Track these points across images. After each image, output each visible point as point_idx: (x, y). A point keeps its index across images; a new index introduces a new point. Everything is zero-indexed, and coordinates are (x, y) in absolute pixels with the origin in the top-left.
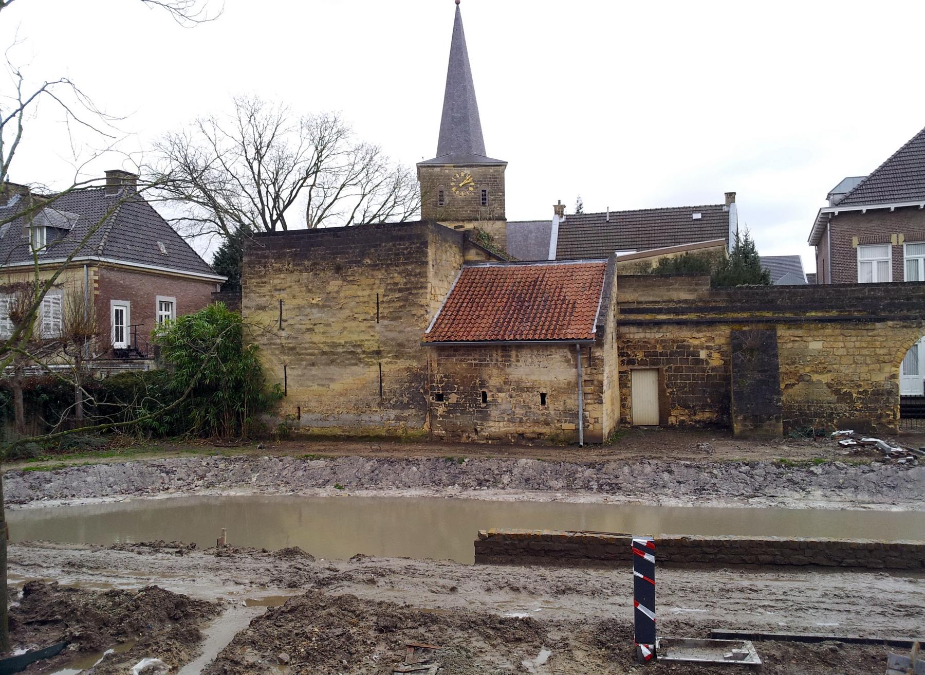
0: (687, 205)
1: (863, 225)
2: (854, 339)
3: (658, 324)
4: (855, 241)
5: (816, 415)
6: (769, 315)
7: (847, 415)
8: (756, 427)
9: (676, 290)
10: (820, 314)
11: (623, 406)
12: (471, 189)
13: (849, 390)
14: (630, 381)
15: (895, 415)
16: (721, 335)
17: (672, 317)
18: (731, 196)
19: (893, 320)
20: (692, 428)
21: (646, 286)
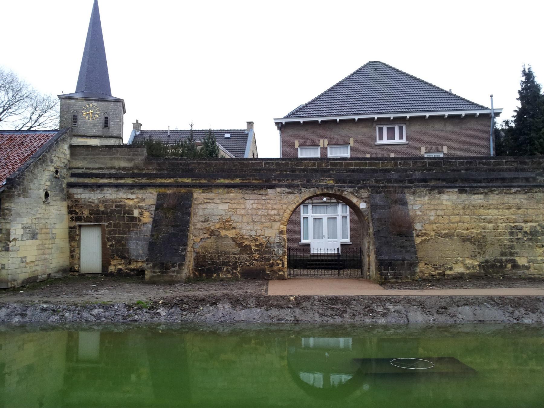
0: (222, 129)
1: (302, 133)
2: (252, 202)
3: (100, 186)
4: (297, 143)
5: (224, 264)
6: (188, 181)
7: (248, 263)
8: (163, 273)
9: (117, 159)
10: (227, 181)
11: (72, 257)
12: (97, 116)
13: (248, 243)
14: (79, 235)
15: (283, 264)
16: (150, 197)
17: (112, 181)
18: (250, 124)
19: (281, 186)
20: (127, 275)
21: (94, 155)
